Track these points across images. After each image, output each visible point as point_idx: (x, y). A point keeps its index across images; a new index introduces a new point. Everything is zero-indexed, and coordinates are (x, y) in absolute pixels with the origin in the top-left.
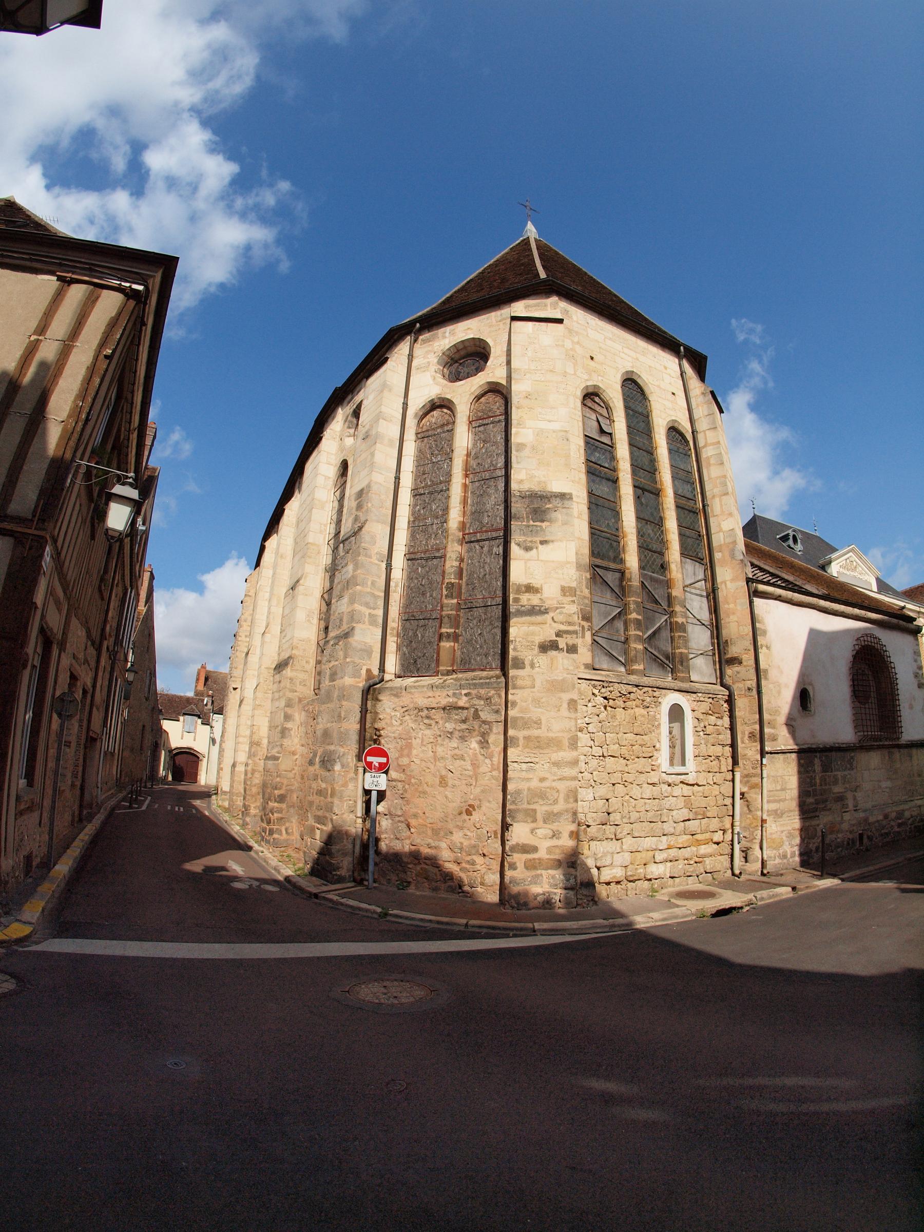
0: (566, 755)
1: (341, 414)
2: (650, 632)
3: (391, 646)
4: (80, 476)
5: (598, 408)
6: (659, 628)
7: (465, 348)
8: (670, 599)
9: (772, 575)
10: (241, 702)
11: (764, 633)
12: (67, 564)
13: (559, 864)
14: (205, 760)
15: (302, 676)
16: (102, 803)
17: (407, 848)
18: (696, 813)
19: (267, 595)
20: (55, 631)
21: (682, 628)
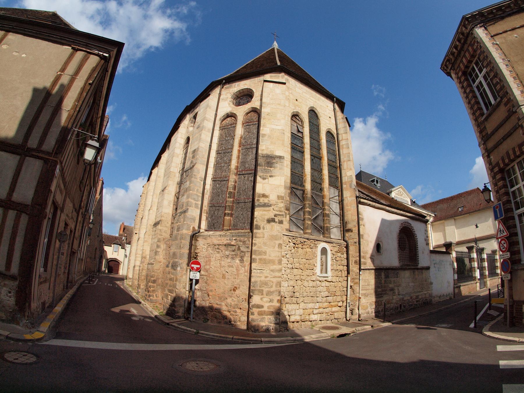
0: (277, 267)
1: (188, 117)
2: (314, 217)
3: (204, 217)
4: (74, 135)
5: (297, 121)
6: (318, 216)
7: (243, 92)
8: (323, 203)
9: (367, 195)
10: (138, 239)
11: (363, 219)
12: (66, 174)
13: (272, 313)
14: (122, 264)
15: (165, 229)
16: (77, 281)
17: (207, 305)
18: (331, 294)
19: (152, 193)
20: (59, 203)
21: (328, 216)
